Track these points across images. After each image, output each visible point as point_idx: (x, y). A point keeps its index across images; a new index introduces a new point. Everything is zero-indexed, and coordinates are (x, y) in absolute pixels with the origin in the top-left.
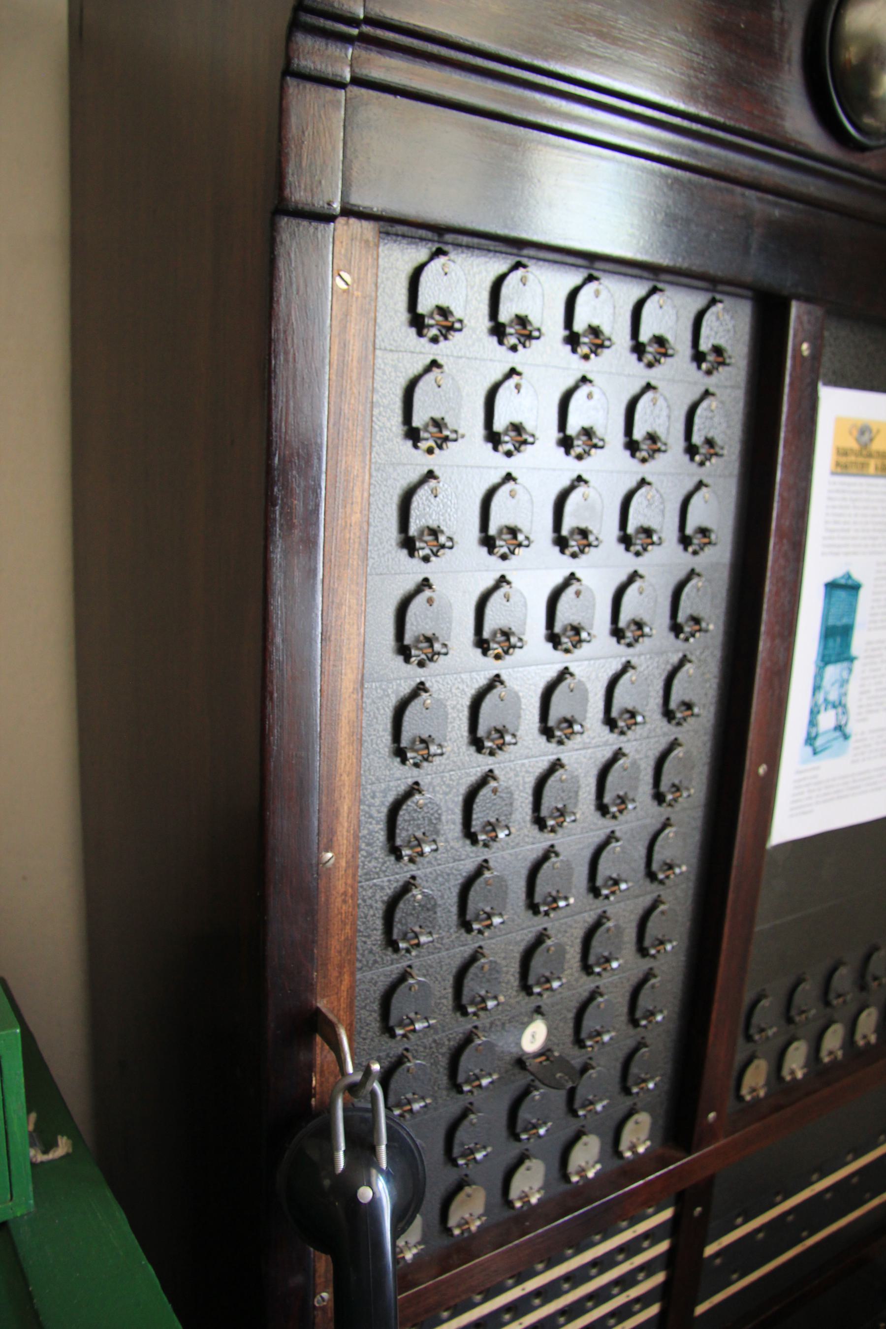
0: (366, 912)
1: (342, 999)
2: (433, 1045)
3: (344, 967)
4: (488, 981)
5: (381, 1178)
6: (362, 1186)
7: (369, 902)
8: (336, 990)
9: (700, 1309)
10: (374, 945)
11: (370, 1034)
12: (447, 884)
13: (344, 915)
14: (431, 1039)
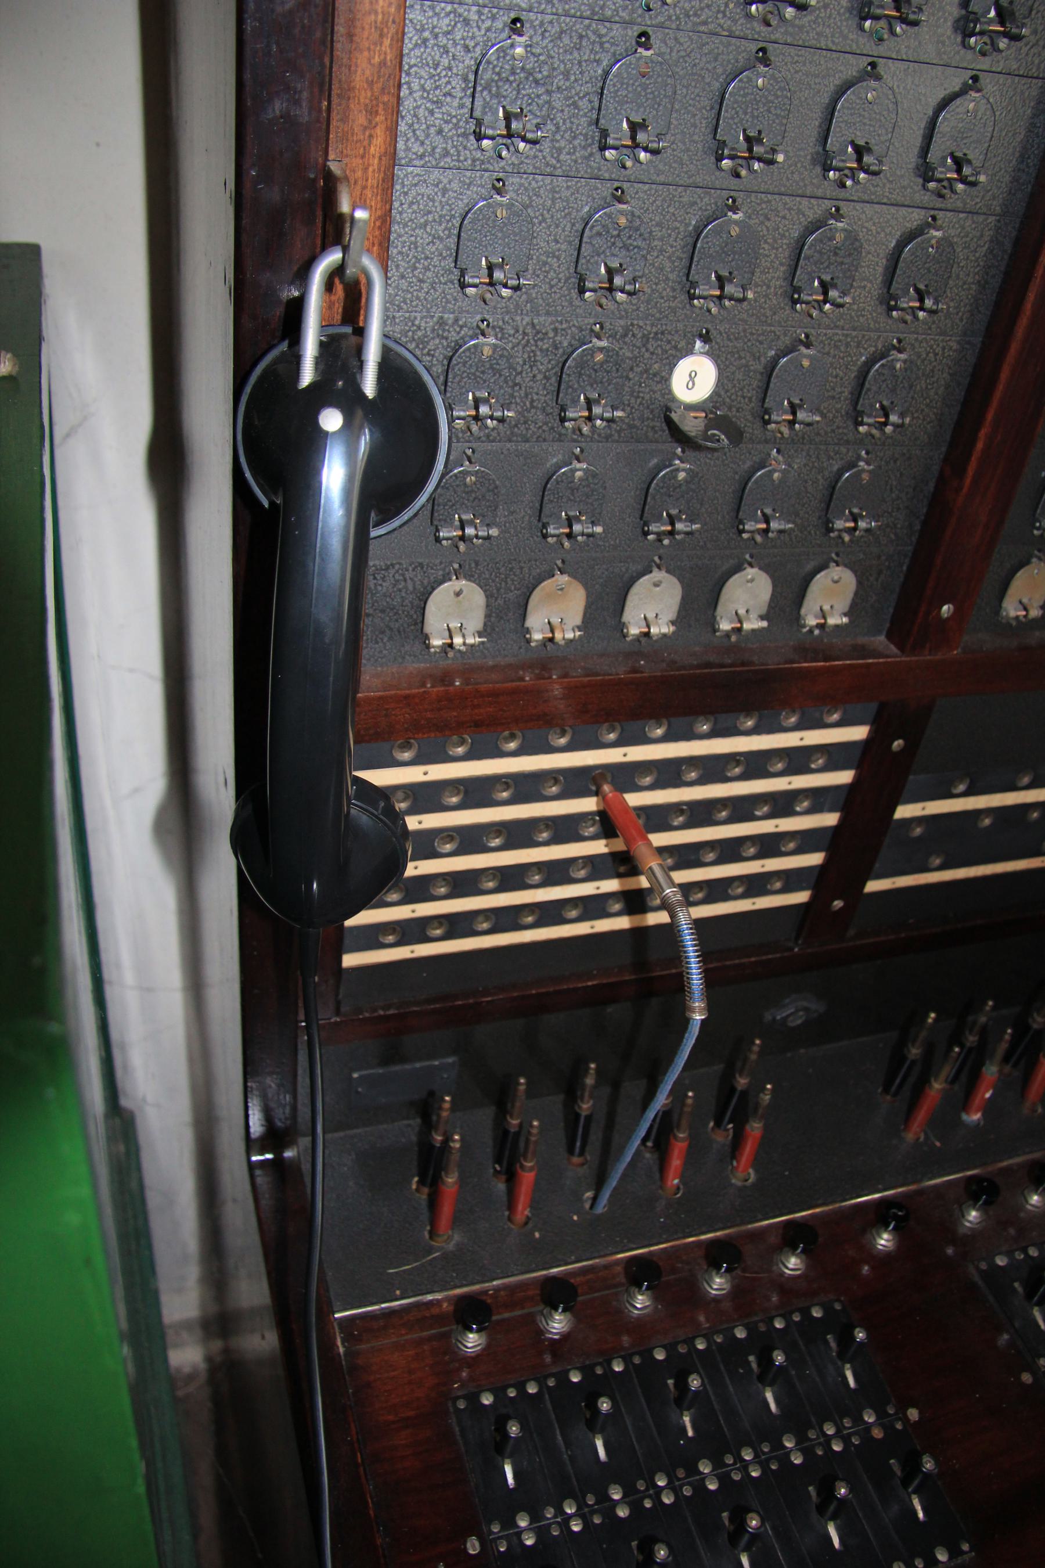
0: (437, 58)
1: (371, 169)
2: (529, 330)
3: (377, 113)
4: (626, 247)
5: (722, 1066)
6: (343, 426)
7: (442, 40)
8: (361, 151)
9: (873, 886)
10: (447, 122)
11: (429, 274)
12: (576, 54)
13: (380, 17)
14: (527, 319)
